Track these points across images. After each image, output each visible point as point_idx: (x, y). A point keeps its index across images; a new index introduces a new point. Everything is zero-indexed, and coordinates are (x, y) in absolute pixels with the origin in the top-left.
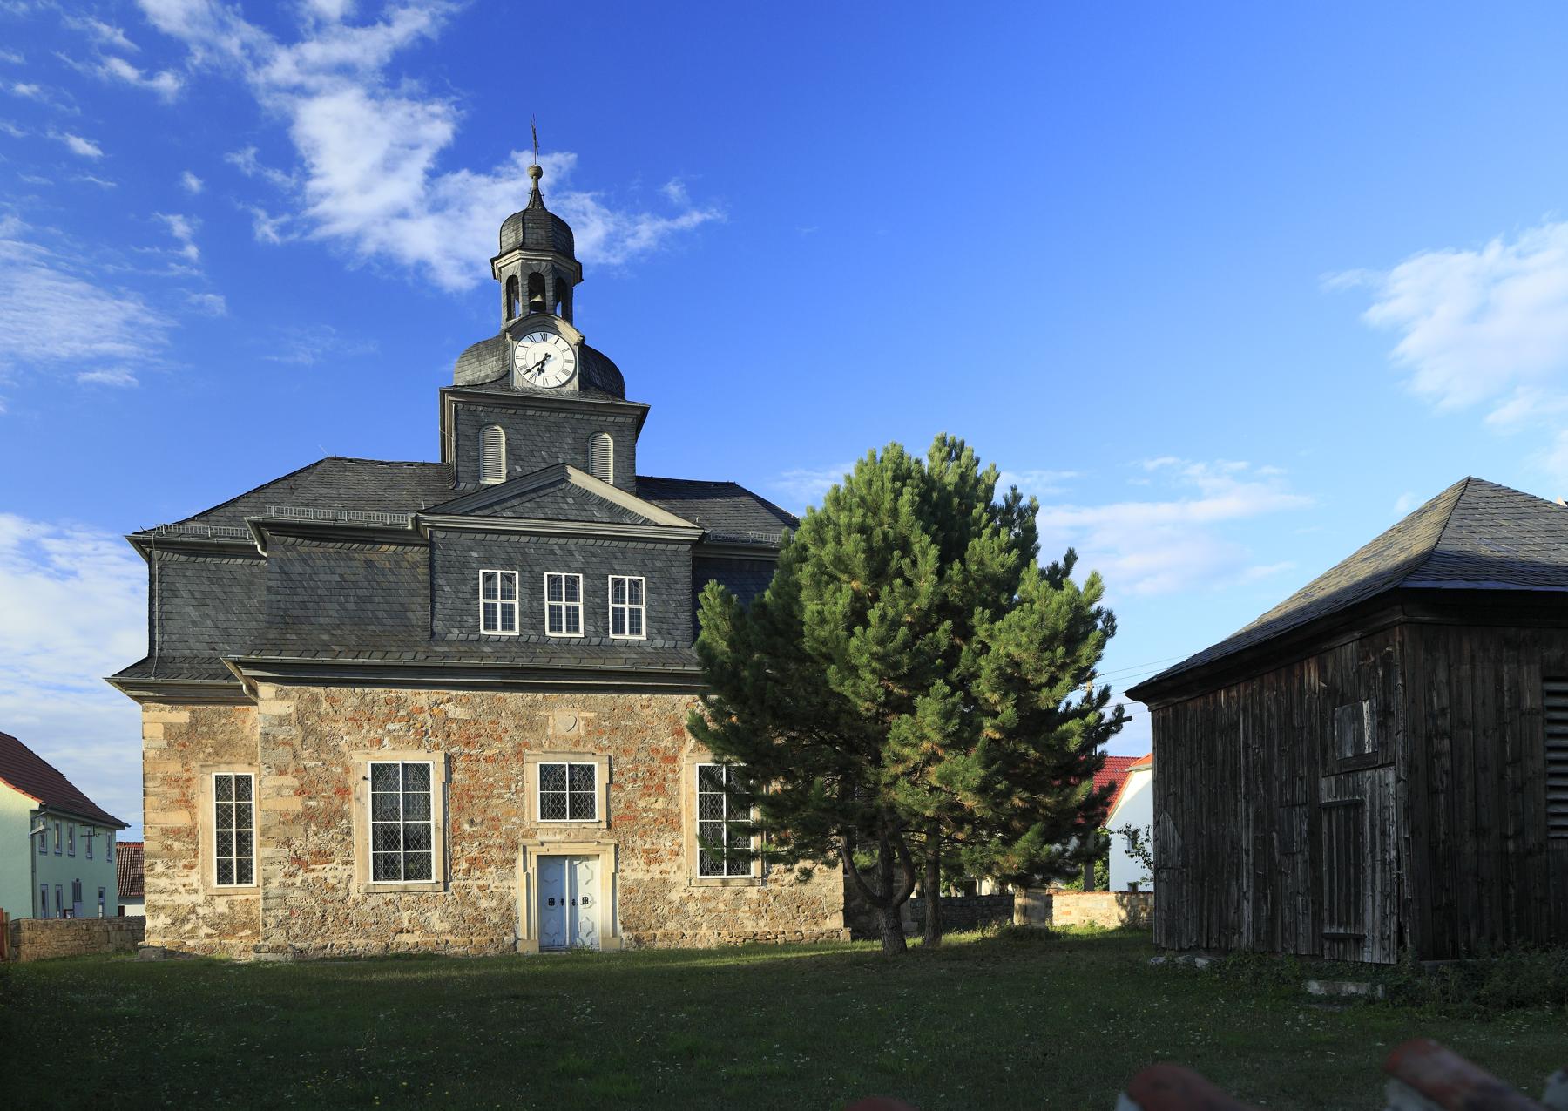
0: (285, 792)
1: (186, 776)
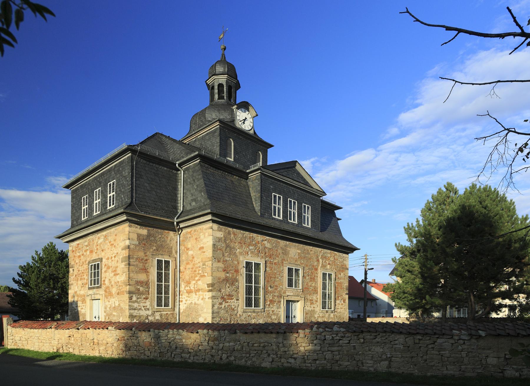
0: (220, 270)
1: (145, 258)
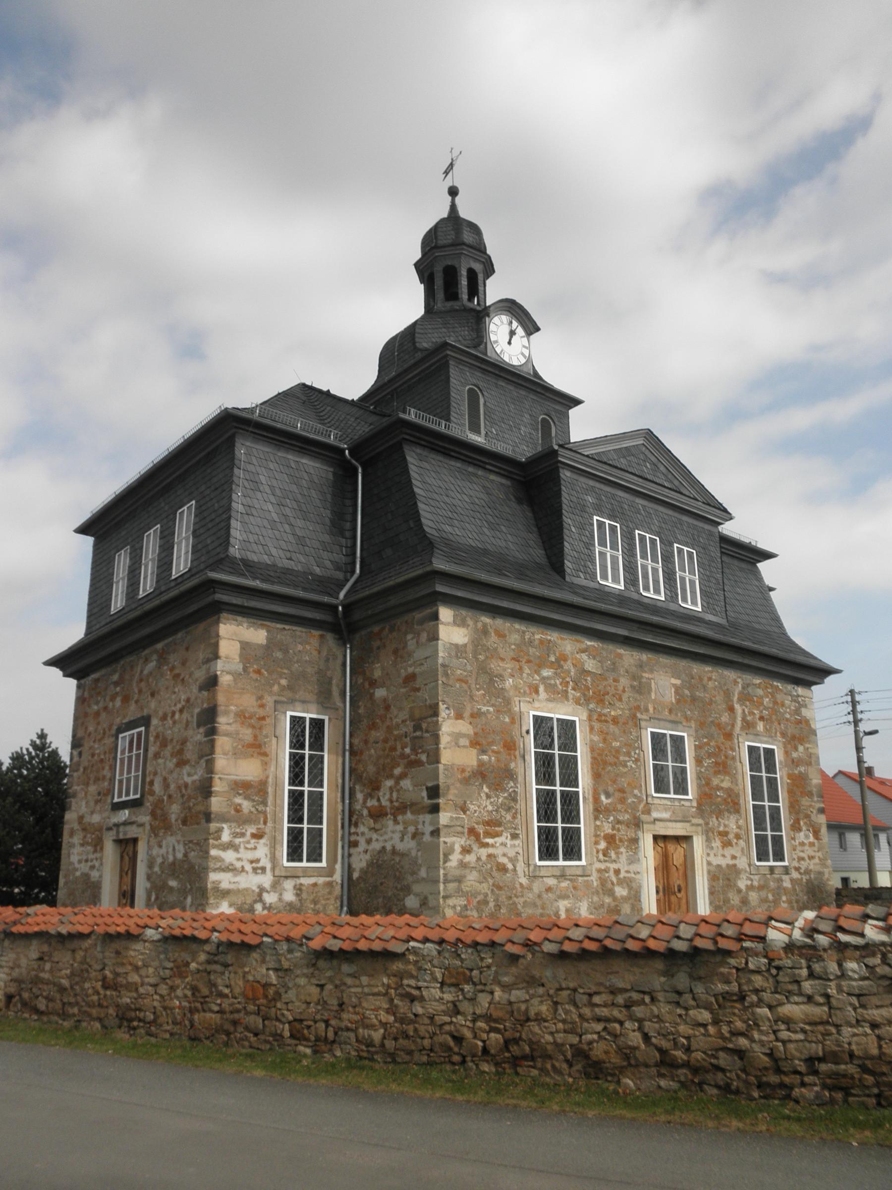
1: (261, 712)
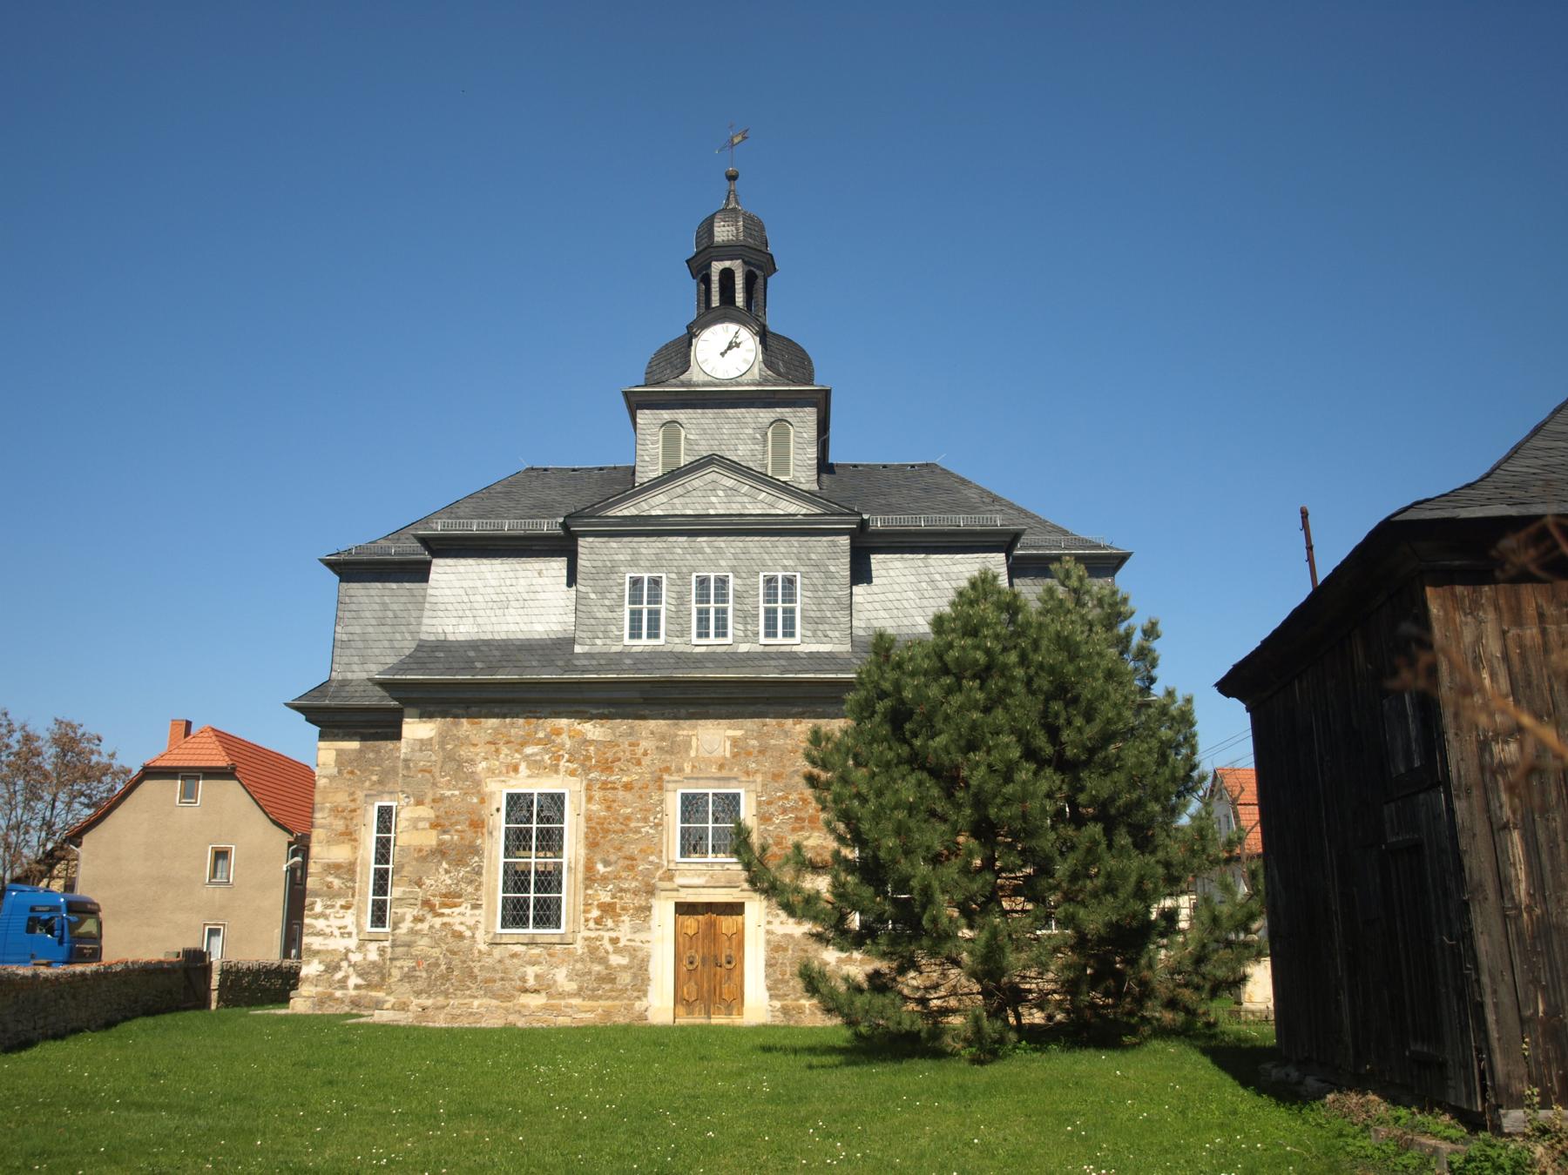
0: (421, 825)
1: (352, 806)
